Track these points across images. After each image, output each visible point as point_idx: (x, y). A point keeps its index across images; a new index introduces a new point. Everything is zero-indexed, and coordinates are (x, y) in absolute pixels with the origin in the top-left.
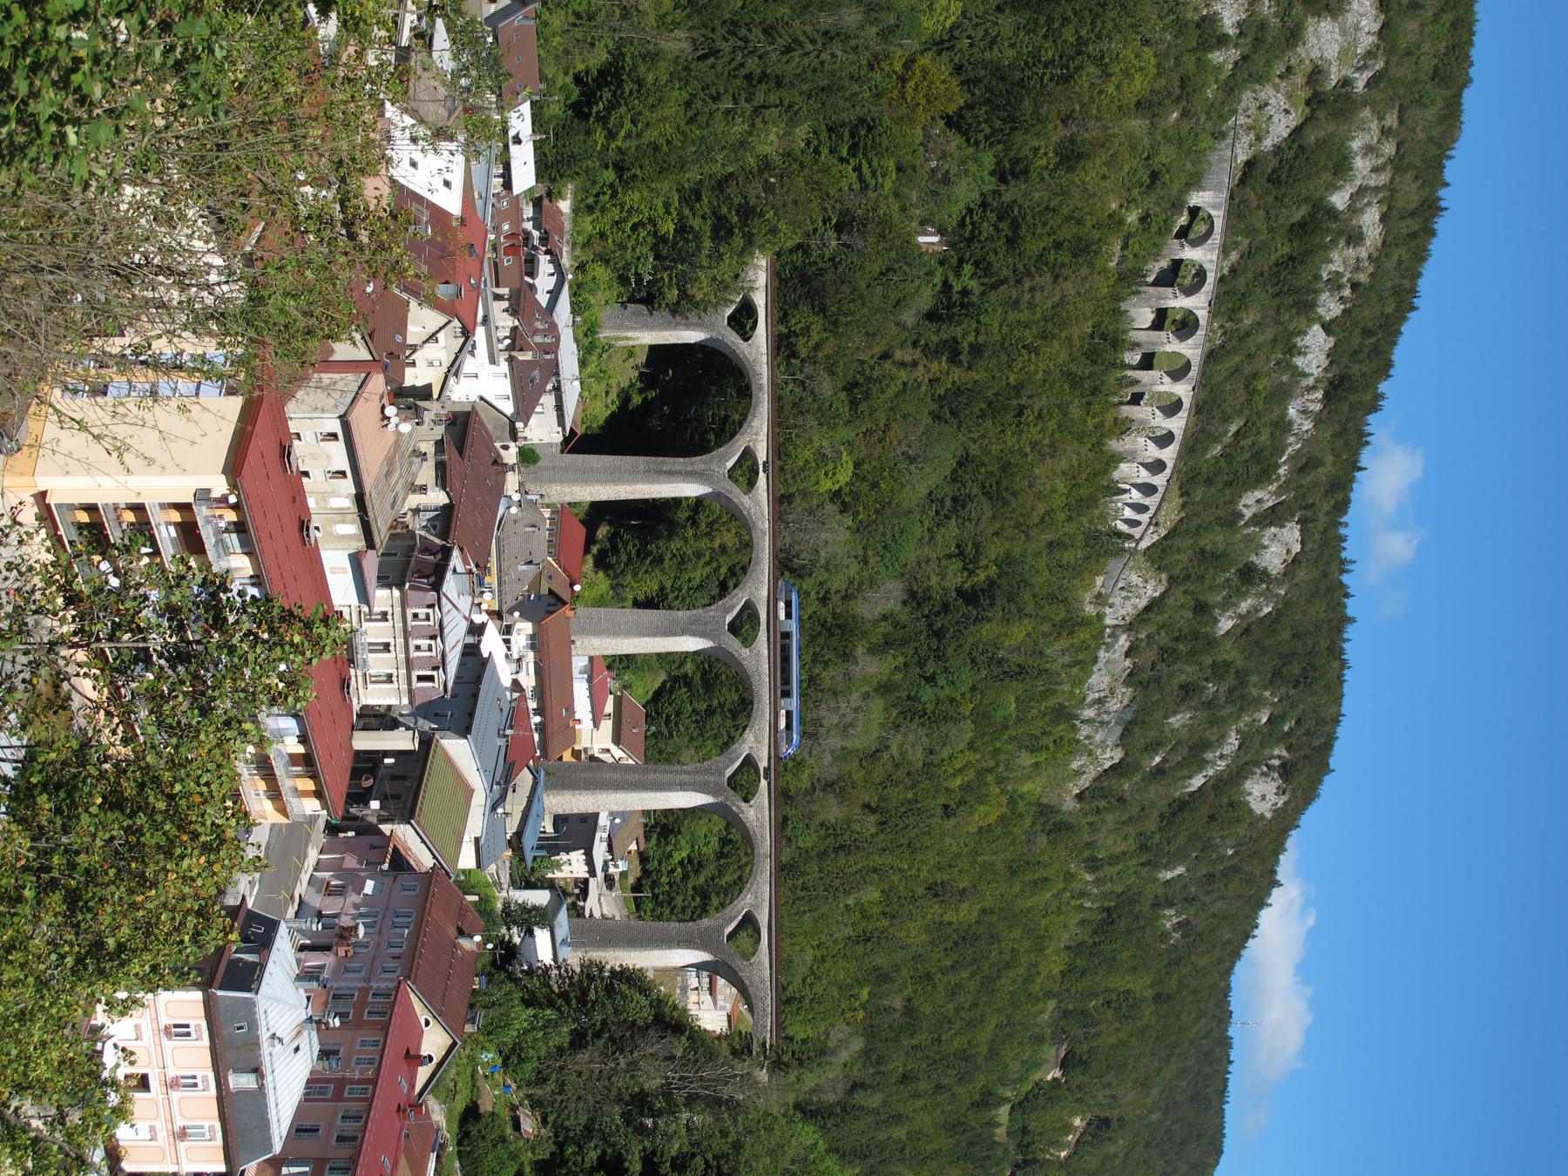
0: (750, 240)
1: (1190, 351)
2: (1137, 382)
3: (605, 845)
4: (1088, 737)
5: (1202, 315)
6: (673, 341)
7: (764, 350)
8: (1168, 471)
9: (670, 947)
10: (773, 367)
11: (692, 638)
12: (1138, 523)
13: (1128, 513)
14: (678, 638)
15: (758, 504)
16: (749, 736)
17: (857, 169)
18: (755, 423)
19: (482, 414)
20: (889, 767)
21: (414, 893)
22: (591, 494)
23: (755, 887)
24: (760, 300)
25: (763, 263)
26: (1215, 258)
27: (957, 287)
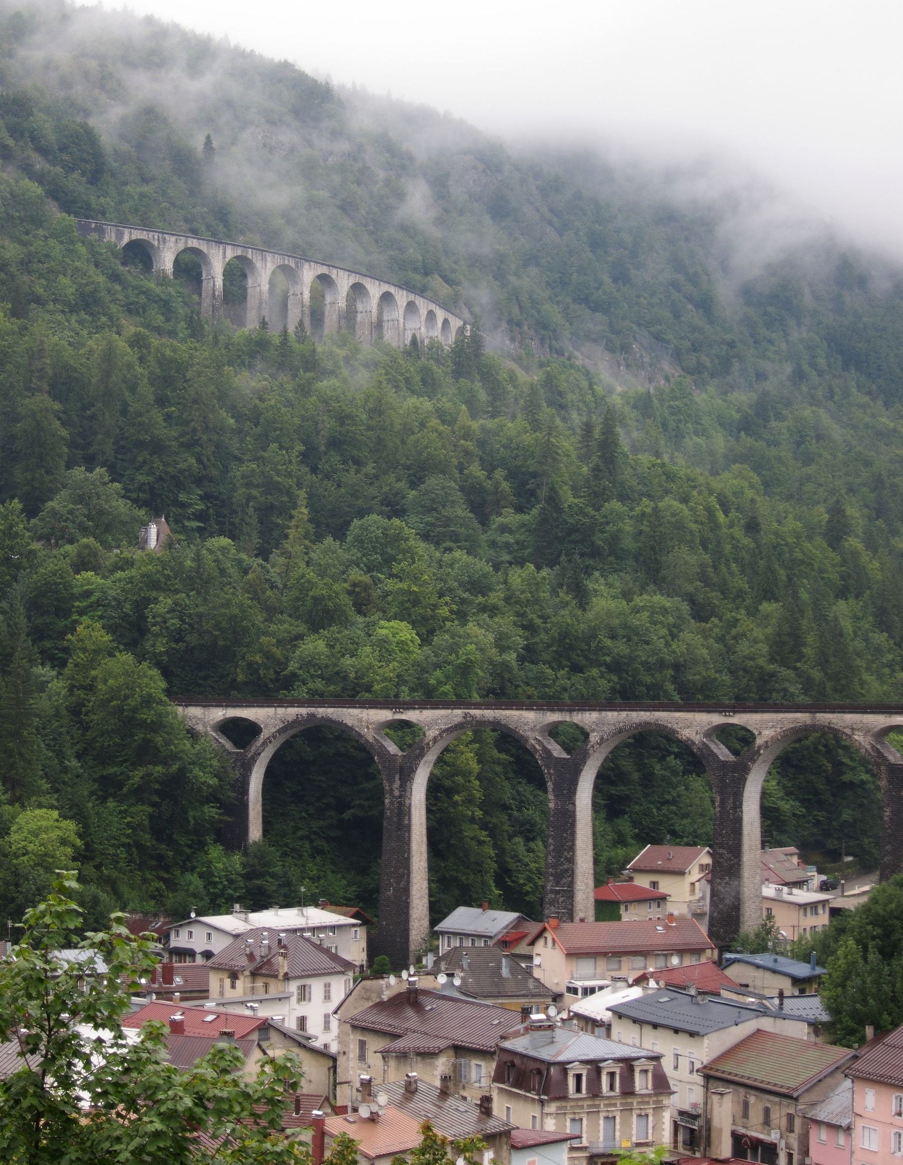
0: (156, 726)
1: (269, 265)
2: (301, 324)
3: (795, 891)
4: (667, 379)
5: (230, 253)
6: (259, 808)
7: (270, 711)
8: (392, 290)
9: (381, 708)
10: (291, 703)
11: (578, 794)
12: (446, 322)
13: (437, 332)
14: (578, 809)
15: (435, 721)
16: (686, 734)
17: (82, 613)
18: (349, 722)
19: (354, 1012)
20: (247, 519)
21: (358, 932)
22: (421, 898)
23: (848, 731)
24: (219, 714)
25: (180, 709)
26: (173, 239)
27: (200, 507)
